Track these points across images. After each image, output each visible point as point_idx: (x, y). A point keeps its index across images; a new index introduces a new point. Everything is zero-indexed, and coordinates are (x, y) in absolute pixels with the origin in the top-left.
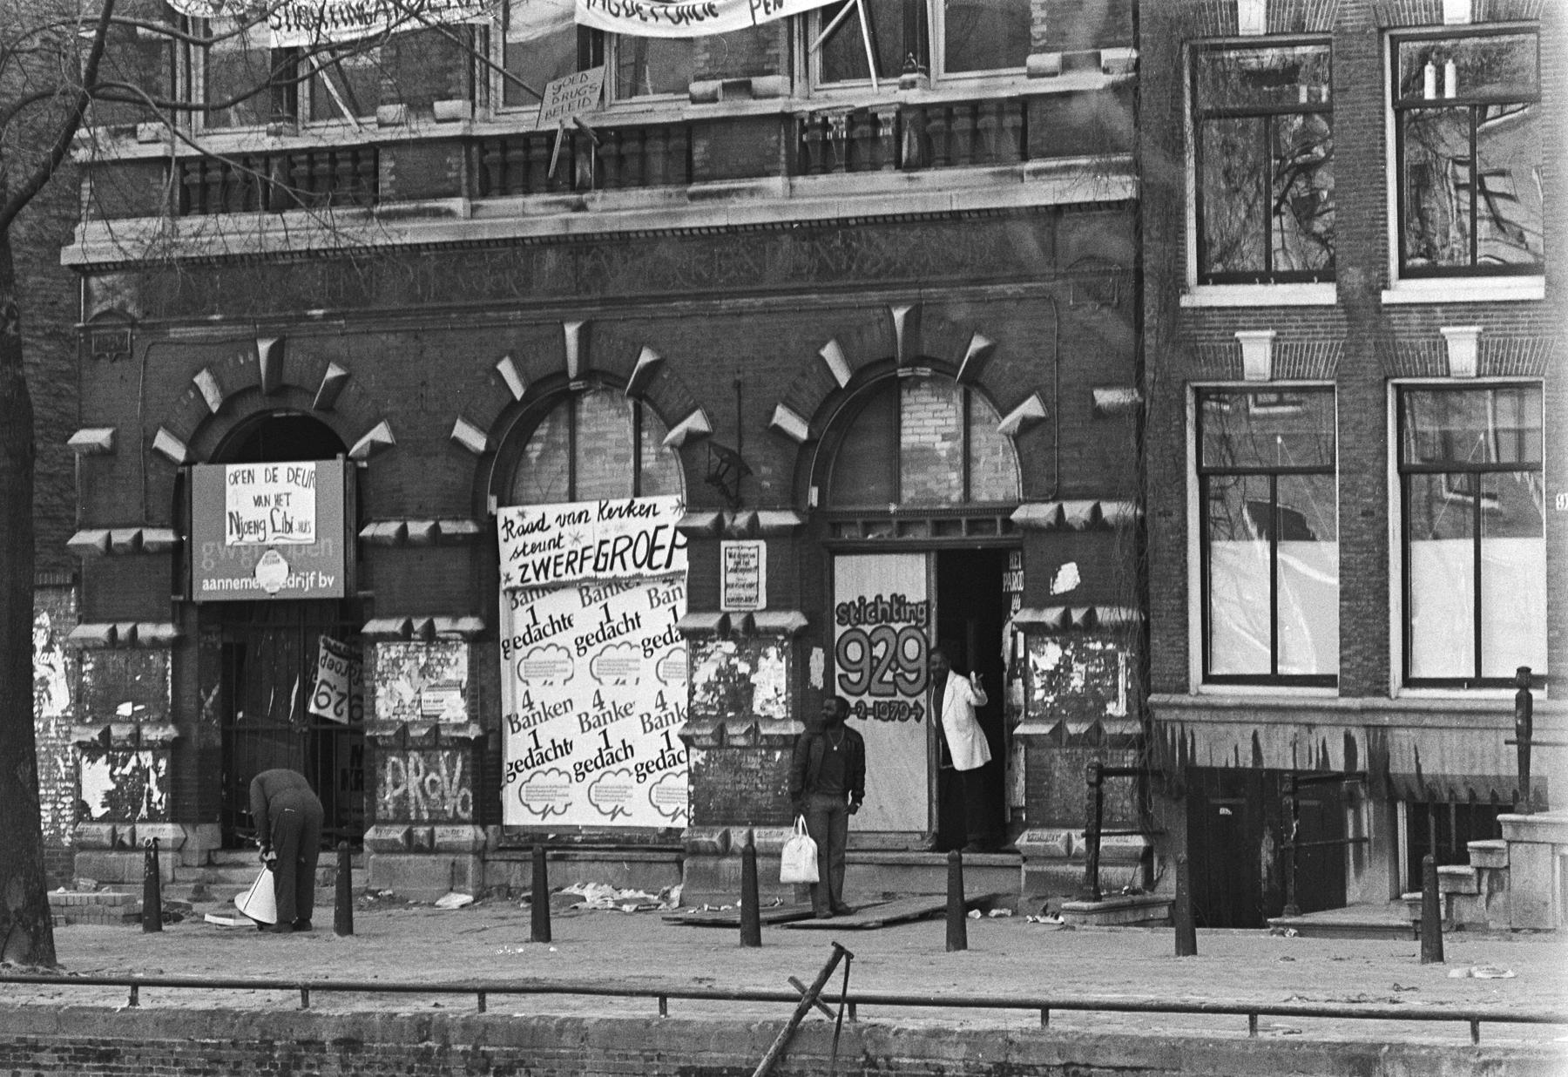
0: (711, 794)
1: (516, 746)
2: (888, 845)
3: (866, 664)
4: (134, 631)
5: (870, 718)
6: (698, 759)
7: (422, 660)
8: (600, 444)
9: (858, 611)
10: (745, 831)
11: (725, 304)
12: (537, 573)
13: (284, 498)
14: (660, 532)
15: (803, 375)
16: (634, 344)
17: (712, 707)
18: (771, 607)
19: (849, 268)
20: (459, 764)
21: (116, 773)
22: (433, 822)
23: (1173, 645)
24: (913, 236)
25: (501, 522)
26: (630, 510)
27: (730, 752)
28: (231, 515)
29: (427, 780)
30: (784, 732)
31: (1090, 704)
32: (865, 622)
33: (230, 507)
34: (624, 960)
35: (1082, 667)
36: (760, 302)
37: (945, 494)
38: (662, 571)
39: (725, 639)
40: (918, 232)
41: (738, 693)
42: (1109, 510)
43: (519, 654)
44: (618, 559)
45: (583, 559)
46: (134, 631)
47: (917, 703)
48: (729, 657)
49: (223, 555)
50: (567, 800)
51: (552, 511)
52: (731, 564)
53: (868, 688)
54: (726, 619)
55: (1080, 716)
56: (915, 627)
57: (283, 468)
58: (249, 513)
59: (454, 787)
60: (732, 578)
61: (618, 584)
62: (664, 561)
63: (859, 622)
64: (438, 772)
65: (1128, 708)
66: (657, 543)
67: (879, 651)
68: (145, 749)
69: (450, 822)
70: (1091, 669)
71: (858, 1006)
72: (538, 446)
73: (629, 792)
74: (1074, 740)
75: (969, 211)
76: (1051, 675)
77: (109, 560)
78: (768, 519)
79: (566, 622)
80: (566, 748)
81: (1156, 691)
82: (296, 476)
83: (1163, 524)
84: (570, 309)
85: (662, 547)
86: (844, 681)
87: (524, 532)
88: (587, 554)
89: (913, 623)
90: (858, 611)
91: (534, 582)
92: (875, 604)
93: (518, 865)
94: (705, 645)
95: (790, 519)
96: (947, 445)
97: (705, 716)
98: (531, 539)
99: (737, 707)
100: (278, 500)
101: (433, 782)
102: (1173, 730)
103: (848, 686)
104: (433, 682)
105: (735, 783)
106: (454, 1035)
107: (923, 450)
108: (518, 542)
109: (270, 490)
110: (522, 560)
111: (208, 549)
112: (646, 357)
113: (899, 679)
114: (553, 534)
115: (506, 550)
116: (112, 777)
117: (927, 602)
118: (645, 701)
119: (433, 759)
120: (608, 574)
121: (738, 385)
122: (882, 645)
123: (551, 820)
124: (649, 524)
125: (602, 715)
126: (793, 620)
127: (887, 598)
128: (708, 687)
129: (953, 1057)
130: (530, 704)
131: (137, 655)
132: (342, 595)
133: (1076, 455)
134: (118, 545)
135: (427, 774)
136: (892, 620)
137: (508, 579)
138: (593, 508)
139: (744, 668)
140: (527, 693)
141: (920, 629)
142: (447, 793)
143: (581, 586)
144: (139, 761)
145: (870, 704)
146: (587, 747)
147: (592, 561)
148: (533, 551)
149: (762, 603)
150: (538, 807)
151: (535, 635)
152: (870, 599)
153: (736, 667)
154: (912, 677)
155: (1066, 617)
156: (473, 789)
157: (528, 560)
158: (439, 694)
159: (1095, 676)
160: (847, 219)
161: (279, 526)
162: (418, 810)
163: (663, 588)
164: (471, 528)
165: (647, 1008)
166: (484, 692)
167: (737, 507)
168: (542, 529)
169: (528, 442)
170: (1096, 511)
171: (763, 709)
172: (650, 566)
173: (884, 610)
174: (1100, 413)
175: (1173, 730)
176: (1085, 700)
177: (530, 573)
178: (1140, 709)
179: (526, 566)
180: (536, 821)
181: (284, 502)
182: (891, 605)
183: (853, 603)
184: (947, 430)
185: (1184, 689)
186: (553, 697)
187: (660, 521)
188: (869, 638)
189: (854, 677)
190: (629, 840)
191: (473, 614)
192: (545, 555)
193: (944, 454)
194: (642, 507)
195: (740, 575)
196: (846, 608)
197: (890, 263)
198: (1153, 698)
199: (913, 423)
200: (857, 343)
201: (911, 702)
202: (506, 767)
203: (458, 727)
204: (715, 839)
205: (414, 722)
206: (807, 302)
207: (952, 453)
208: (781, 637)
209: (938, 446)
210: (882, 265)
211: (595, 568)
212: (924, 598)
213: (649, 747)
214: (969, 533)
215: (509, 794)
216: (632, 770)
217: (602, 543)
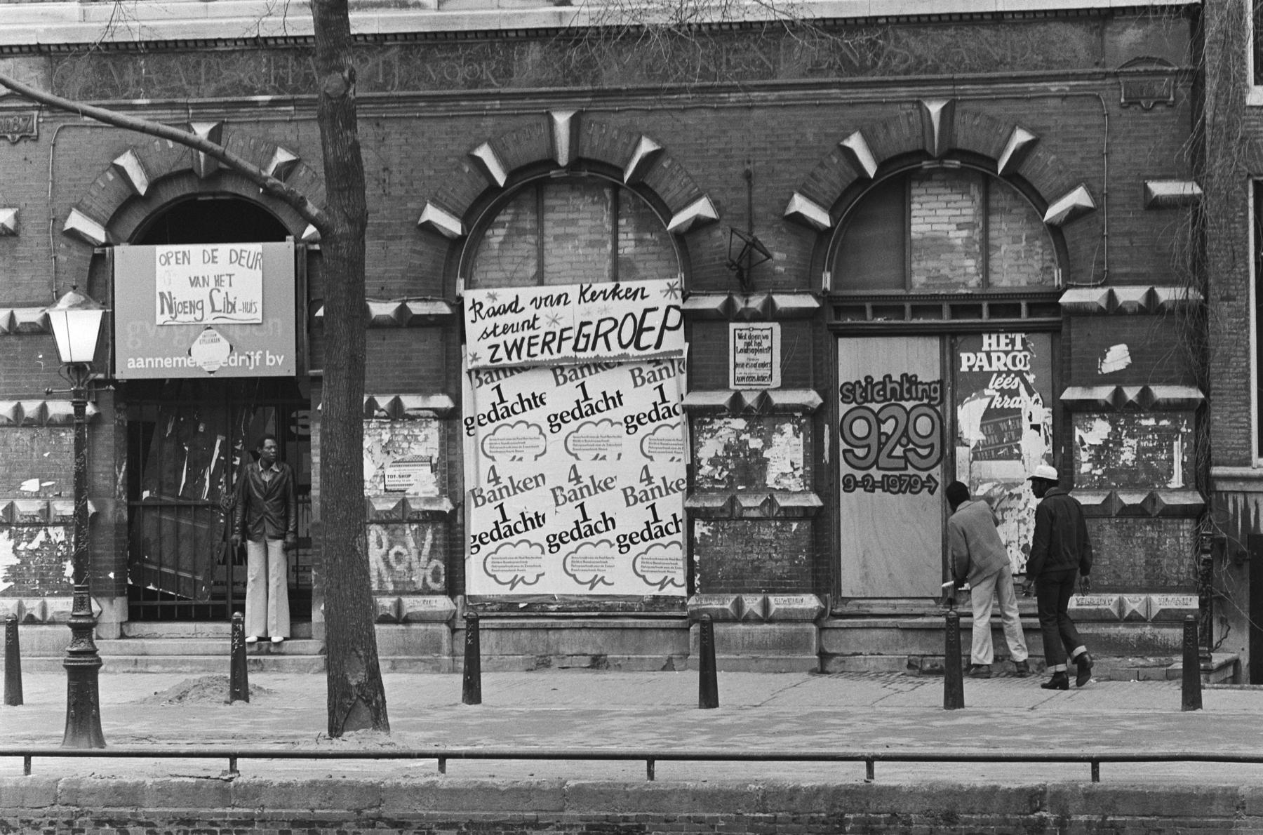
0: (720, 564)
1: (479, 520)
2: (899, 611)
3: (873, 441)
4: (43, 409)
5: (878, 491)
6: (705, 530)
7: (386, 437)
8: (570, 230)
9: (865, 390)
10: (760, 598)
11: (733, 97)
12: (509, 354)
13: (226, 279)
14: (648, 315)
15: (822, 165)
16: (631, 135)
17: (721, 482)
18: (786, 385)
19: (875, 64)
20: (429, 537)
21: (21, 547)
22: (398, 593)
23: (1236, 421)
24: (947, 36)
25: (468, 304)
26: (615, 293)
27: (739, 524)
28: (162, 294)
29: (392, 553)
30: (807, 504)
31: (1149, 475)
32: (873, 400)
33: (161, 287)
34: (624, 720)
35: (1133, 442)
36: (773, 96)
37: (962, 279)
38: (651, 351)
39: (735, 417)
40: (952, 31)
41: (749, 469)
42: (1165, 294)
43: (482, 432)
44: (601, 341)
45: (561, 339)
46: (43, 409)
47: (929, 476)
48: (738, 433)
49: (152, 333)
50: (540, 571)
51: (527, 294)
52: (741, 344)
53: (876, 462)
54: (737, 397)
55: (1132, 487)
56: (928, 405)
57: (224, 249)
58: (183, 293)
59: (424, 559)
60: (741, 358)
61: (600, 365)
62: (654, 342)
63: (866, 400)
64: (405, 545)
65: (1184, 480)
66: (645, 326)
67: (888, 427)
68: (55, 524)
69: (417, 593)
70: (1144, 444)
71: (1101, 765)
72: (501, 232)
73: (610, 562)
74: (1128, 511)
75: (1013, 13)
76: (1099, 449)
77: (13, 339)
78: (784, 301)
79: (537, 400)
80: (538, 520)
81: (1217, 465)
82: (239, 258)
83: (1225, 307)
84: (562, 99)
85: (652, 329)
86: (849, 455)
87: (495, 314)
88: (565, 335)
89: (926, 401)
90: (865, 390)
91: (505, 361)
92: (884, 383)
93: (494, 634)
94: (711, 422)
95: (809, 302)
96: (965, 233)
97: (712, 489)
98: (501, 320)
99: (749, 481)
100: (218, 280)
101: (398, 554)
102: (1235, 502)
103: (854, 461)
104: (398, 458)
105: (744, 553)
106: (1074, 806)
107: (934, 239)
108: (489, 323)
109: (211, 271)
110: (492, 340)
111: (134, 328)
112: (646, 147)
113: (911, 455)
114: (528, 314)
115: (473, 330)
116: (15, 551)
117: (941, 382)
118: (628, 474)
119: (399, 532)
120: (589, 354)
121: (748, 176)
122: (892, 422)
123: (520, 589)
124: (637, 307)
125: (579, 488)
126: (810, 397)
127: (896, 378)
128: (714, 462)
129: (913, 809)
130: (497, 479)
131: (45, 432)
132: (293, 374)
133: (1127, 243)
134: (23, 324)
135: (391, 546)
136: (902, 398)
137: (475, 358)
138: (573, 291)
139: (755, 443)
140: (493, 468)
141: (933, 407)
142: (415, 565)
143: (556, 369)
144: (48, 536)
145: (878, 478)
146: (562, 519)
147: (572, 342)
148: (504, 332)
149: (777, 380)
150: (505, 577)
151: (501, 412)
152: (878, 378)
153: (746, 442)
154: (924, 452)
155: (1118, 394)
156: (445, 561)
157: (499, 340)
158: (405, 470)
159: (1146, 450)
160: (877, 18)
161: (219, 306)
162: (381, 582)
163: (646, 369)
164: (444, 309)
165: (1082, 772)
166: (448, 470)
167: (748, 289)
168: (515, 311)
169: (488, 228)
170: (1151, 295)
171: (777, 482)
172: (637, 347)
173: (893, 390)
174: (1158, 205)
175: (1235, 502)
176: (1137, 472)
177: (501, 353)
178: (1199, 478)
179: (497, 346)
180: (505, 591)
181: (226, 283)
182: (901, 385)
183: (859, 382)
184: (962, 220)
185: (1247, 462)
186: (522, 472)
187: (648, 303)
188: (876, 415)
189: (860, 452)
190: (610, 608)
191: (444, 392)
192: (518, 336)
193: (959, 242)
194: (629, 290)
195: (752, 355)
196: (852, 387)
197: (920, 60)
198: (1216, 471)
199: (924, 212)
200: (882, 136)
201: (924, 475)
202: (469, 541)
203: (429, 500)
204: (728, 605)
205: (376, 496)
206: (828, 97)
207: (969, 241)
208: (798, 414)
209: (951, 235)
210: (912, 61)
211: (575, 348)
212: (937, 377)
213: (632, 520)
214: (1030, 315)
215: (473, 565)
216: (614, 541)
217: (583, 324)
